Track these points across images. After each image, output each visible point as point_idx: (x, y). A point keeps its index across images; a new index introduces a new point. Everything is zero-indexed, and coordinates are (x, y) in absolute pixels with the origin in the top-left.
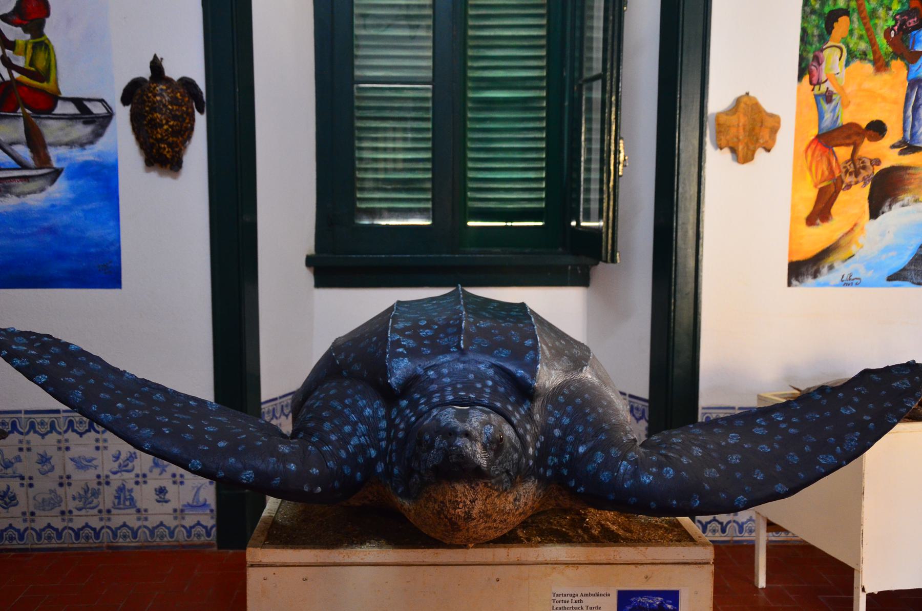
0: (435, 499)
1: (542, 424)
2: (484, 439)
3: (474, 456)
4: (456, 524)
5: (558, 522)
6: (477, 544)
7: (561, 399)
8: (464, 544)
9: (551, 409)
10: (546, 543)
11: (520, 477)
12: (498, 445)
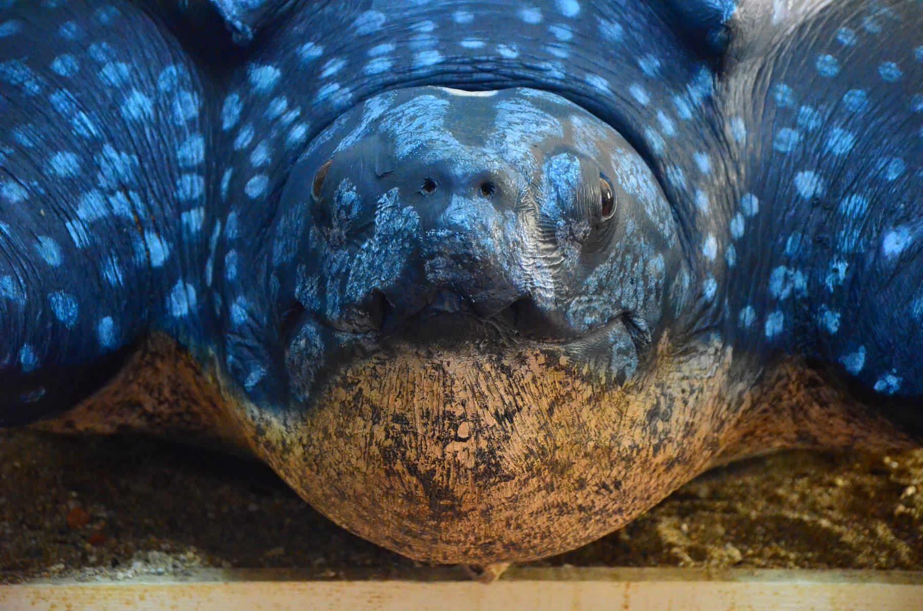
0: (374, 407)
1: (752, 155)
2: (548, 205)
3: (512, 260)
4: (446, 492)
5: (803, 497)
6: (521, 566)
7: (824, 62)
8: (476, 562)
9: (789, 101)
10: (759, 566)
11: (670, 337)
12: (596, 226)
